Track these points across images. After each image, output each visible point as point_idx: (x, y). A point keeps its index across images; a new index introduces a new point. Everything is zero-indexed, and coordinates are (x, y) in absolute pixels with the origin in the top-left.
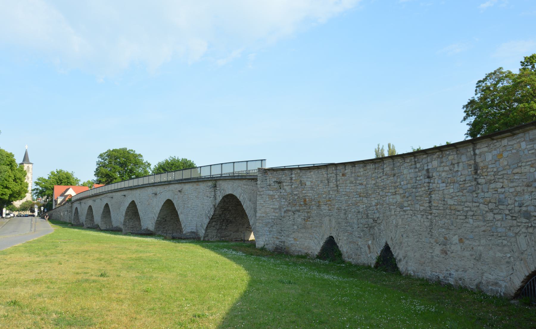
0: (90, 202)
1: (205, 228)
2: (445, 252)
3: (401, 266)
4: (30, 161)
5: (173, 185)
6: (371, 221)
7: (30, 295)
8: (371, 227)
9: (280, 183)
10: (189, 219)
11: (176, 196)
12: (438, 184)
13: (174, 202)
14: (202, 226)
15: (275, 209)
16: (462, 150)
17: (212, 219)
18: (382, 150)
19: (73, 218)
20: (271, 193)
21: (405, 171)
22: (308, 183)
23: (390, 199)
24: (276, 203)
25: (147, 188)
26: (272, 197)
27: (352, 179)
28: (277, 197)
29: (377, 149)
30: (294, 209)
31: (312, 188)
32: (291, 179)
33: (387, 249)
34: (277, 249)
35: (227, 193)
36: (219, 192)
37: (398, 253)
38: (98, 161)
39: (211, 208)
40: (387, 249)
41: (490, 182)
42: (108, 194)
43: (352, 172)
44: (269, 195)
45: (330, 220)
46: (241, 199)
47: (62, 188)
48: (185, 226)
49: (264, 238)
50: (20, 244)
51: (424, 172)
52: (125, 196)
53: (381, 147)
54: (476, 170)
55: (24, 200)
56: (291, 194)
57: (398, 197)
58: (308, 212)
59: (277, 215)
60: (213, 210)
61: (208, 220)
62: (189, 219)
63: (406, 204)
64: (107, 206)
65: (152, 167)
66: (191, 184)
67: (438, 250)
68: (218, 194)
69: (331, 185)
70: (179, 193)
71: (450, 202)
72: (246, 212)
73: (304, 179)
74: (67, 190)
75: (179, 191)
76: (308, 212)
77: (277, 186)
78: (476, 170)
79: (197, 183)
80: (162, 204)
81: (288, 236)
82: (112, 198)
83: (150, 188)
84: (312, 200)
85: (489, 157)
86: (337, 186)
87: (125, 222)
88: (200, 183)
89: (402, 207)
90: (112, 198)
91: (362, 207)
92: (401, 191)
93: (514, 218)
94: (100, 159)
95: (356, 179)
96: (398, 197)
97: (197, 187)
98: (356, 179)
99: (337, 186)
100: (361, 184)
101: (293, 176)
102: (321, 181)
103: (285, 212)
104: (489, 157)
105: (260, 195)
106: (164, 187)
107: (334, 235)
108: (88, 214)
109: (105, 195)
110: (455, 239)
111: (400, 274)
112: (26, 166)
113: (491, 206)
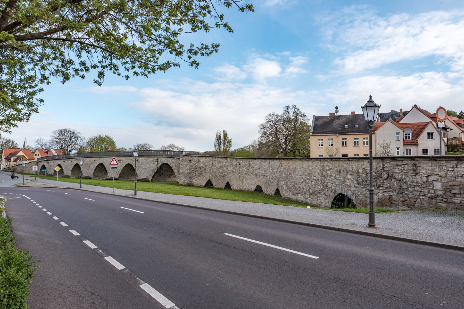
1: (152, 176)
2: (242, 183)
3: (232, 187)
6: (223, 175)
8: (223, 177)
9: (190, 161)
10: (143, 173)
12: (241, 167)
14: (150, 176)
15: (188, 170)
16: (247, 160)
17: (156, 173)
18: (220, 134)
20: (186, 164)
21: (234, 162)
22: (201, 162)
23: (229, 169)
24: (188, 168)
26: (186, 165)
27: (218, 162)
28: (188, 165)
29: (217, 133)
30: (195, 170)
31: (203, 163)
32: (195, 160)
33: (228, 182)
34: (188, 184)
35: (164, 163)
36: (160, 162)
37: (231, 184)
38: (51, 135)
39: (155, 168)
40: (228, 182)
41: (251, 168)
43: (218, 160)
44: (185, 165)
45: (209, 174)
46: (171, 165)
48: (140, 176)
49: (183, 180)
51: (239, 163)
52: (94, 160)
53: (219, 132)
54: (249, 165)
56: (195, 165)
57: (232, 169)
58: (201, 171)
59: (188, 172)
60: (156, 169)
61: (154, 173)
62: (143, 173)
63: (234, 171)
65: (86, 139)
66: (144, 158)
67: (241, 183)
68: (159, 162)
69: (210, 163)
71: (244, 171)
72: (174, 170)
73: (200, 160)
76: (201, 171)
77: (189, 161)
78: (249, 165)
81: (193, 179)
84: (203, 167)
85: (252, 163)
86: (212, 164)
87: (94, 173)
89: (233, 171)
91: (220, 171)
92: (233, 167)
93: (255, 176)
94: (52, 134)
95: (219, 162)
96: (232, 169)
97: (147, 159)
98: (219, 162)
99: (212, 164)
100: (221, 164)
101: (196, 159)
102: (207, 161)
103: (192, 171)
104: (252, 163)
105: (181, 164)
106: (126, 158)
107: (211, 179)
110: (245, 180)
111: (231, 189)
113: (252, 173)
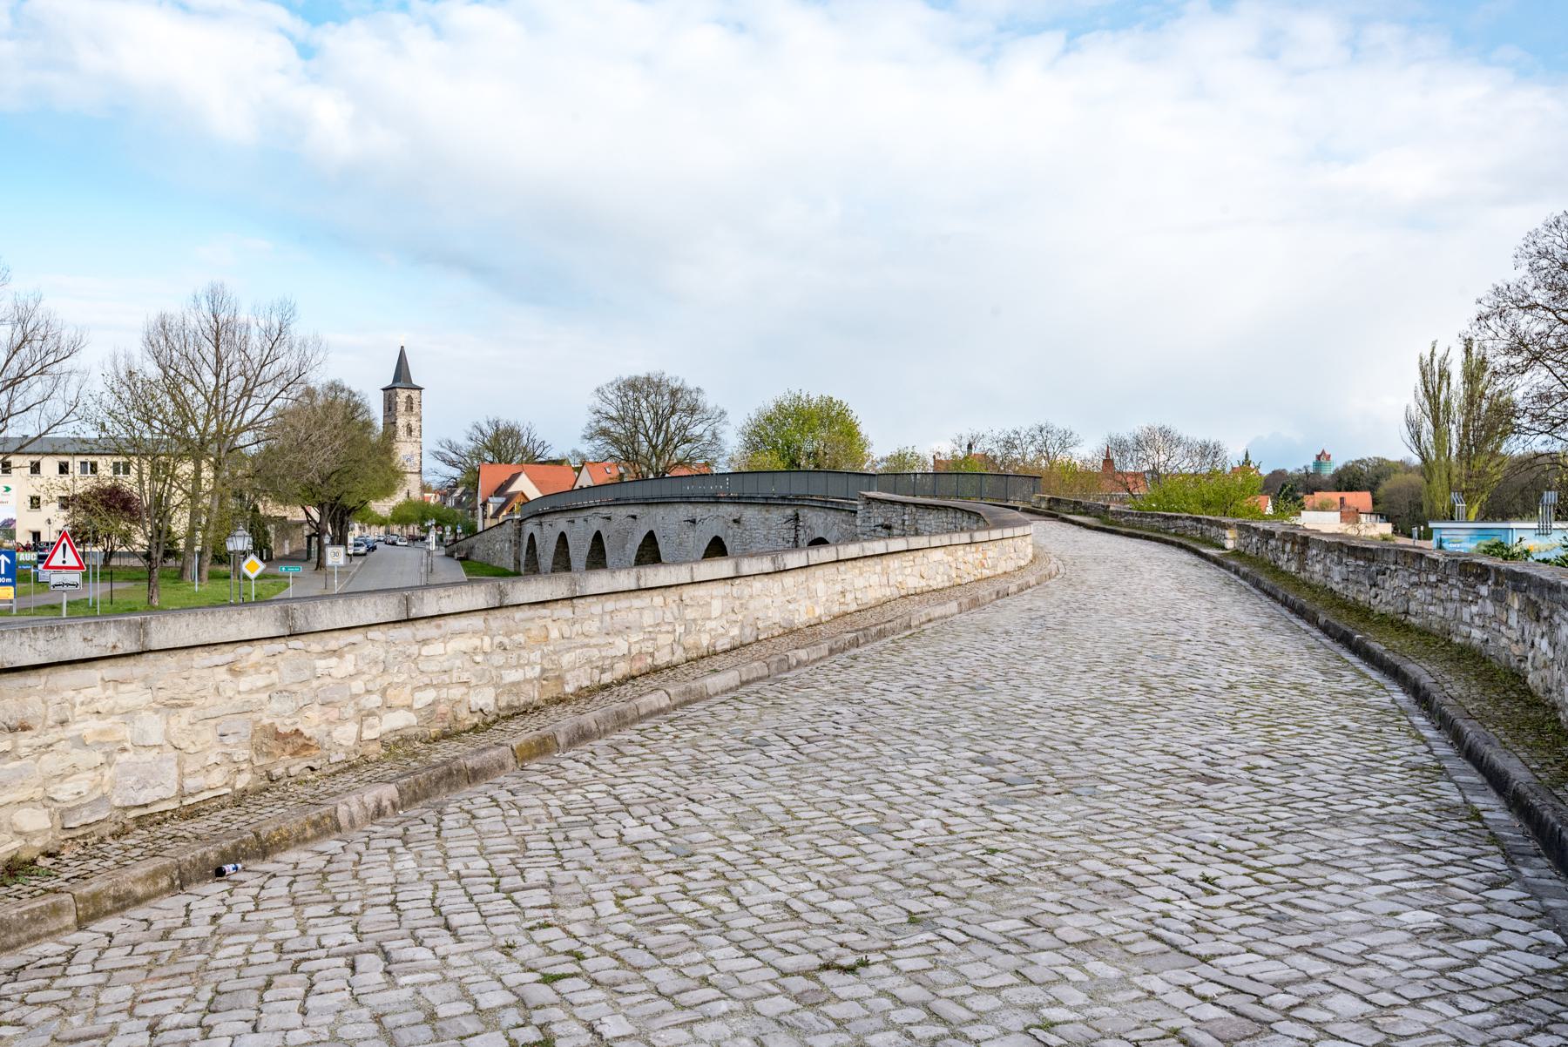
0: (561, 524)
4: (415, 382)
5: (725, 506)
7: (408, 464)
11: (730, 532)
13: (726, 544)
19: (523, 560)
25: (676, 506)
32: (904, 521)
42: (601, 510)
47: (501, 473)
50: (954, 1011)
52: (634, 517)
55: (399, 498)
64: (598, 537)
70: (736, 526)
74: (514, 477)
75: (735, 521)
79: (766, 508)
80: (706, 545)
82: (609, 518)
83: (683, 506)
88: (772, 508)
90: (609, 518)
101: (906, 517)
108: (557, 553)
109: (594, 510)
112: (416, 706)
